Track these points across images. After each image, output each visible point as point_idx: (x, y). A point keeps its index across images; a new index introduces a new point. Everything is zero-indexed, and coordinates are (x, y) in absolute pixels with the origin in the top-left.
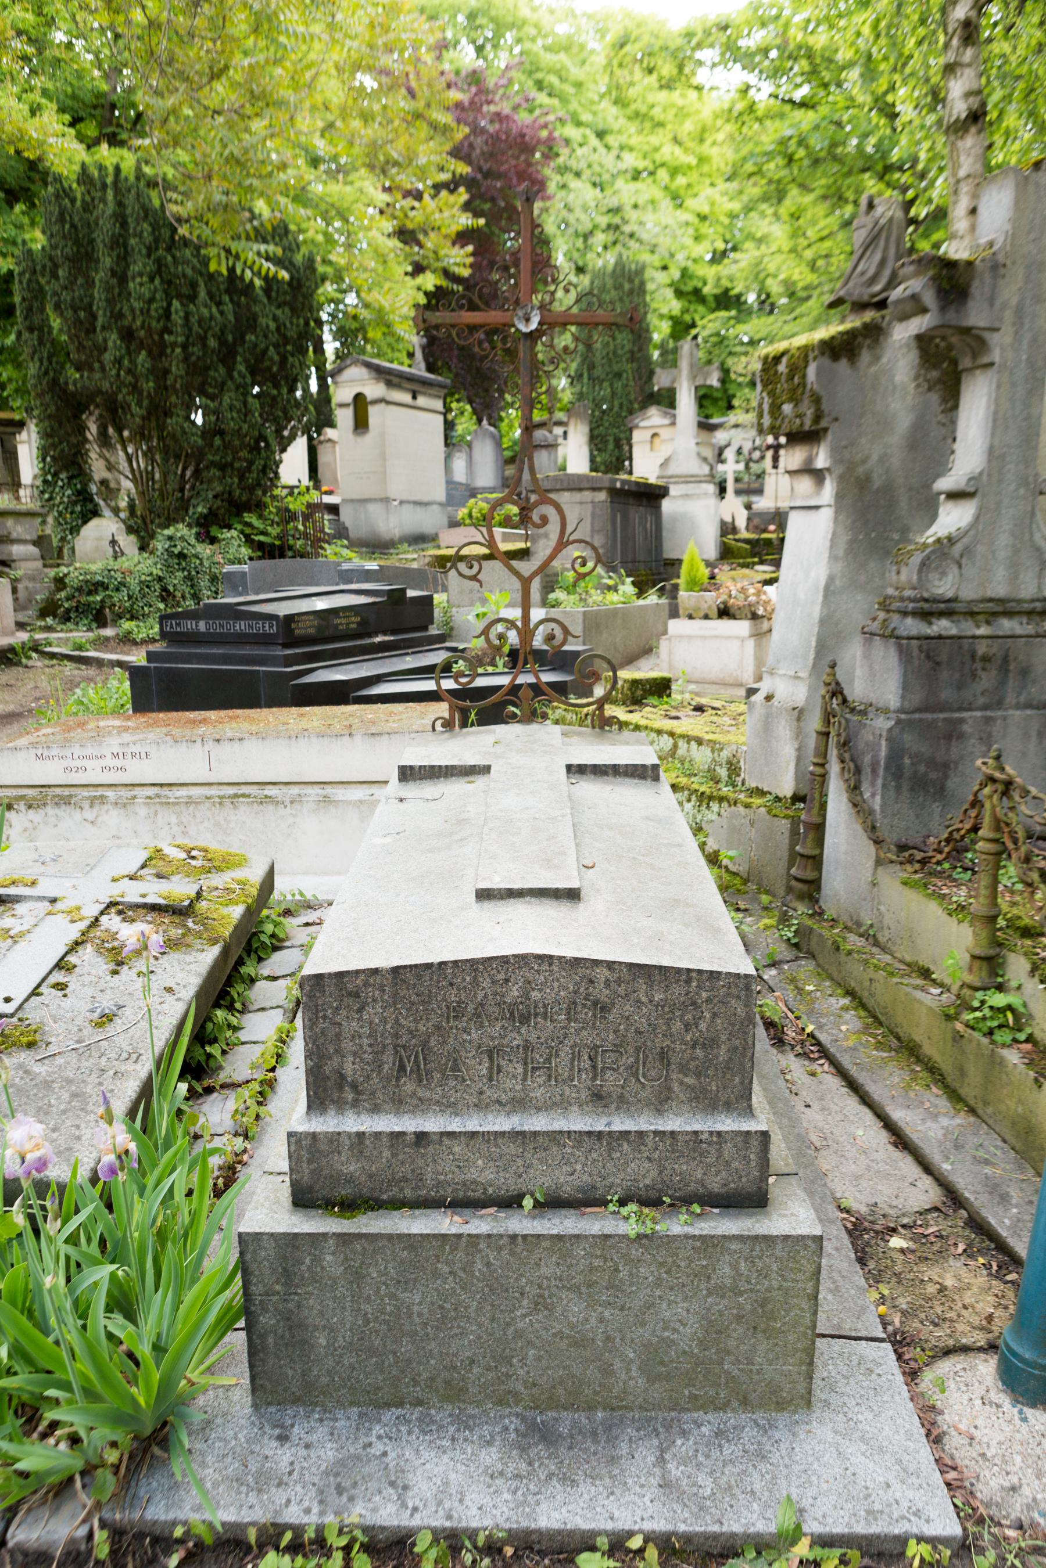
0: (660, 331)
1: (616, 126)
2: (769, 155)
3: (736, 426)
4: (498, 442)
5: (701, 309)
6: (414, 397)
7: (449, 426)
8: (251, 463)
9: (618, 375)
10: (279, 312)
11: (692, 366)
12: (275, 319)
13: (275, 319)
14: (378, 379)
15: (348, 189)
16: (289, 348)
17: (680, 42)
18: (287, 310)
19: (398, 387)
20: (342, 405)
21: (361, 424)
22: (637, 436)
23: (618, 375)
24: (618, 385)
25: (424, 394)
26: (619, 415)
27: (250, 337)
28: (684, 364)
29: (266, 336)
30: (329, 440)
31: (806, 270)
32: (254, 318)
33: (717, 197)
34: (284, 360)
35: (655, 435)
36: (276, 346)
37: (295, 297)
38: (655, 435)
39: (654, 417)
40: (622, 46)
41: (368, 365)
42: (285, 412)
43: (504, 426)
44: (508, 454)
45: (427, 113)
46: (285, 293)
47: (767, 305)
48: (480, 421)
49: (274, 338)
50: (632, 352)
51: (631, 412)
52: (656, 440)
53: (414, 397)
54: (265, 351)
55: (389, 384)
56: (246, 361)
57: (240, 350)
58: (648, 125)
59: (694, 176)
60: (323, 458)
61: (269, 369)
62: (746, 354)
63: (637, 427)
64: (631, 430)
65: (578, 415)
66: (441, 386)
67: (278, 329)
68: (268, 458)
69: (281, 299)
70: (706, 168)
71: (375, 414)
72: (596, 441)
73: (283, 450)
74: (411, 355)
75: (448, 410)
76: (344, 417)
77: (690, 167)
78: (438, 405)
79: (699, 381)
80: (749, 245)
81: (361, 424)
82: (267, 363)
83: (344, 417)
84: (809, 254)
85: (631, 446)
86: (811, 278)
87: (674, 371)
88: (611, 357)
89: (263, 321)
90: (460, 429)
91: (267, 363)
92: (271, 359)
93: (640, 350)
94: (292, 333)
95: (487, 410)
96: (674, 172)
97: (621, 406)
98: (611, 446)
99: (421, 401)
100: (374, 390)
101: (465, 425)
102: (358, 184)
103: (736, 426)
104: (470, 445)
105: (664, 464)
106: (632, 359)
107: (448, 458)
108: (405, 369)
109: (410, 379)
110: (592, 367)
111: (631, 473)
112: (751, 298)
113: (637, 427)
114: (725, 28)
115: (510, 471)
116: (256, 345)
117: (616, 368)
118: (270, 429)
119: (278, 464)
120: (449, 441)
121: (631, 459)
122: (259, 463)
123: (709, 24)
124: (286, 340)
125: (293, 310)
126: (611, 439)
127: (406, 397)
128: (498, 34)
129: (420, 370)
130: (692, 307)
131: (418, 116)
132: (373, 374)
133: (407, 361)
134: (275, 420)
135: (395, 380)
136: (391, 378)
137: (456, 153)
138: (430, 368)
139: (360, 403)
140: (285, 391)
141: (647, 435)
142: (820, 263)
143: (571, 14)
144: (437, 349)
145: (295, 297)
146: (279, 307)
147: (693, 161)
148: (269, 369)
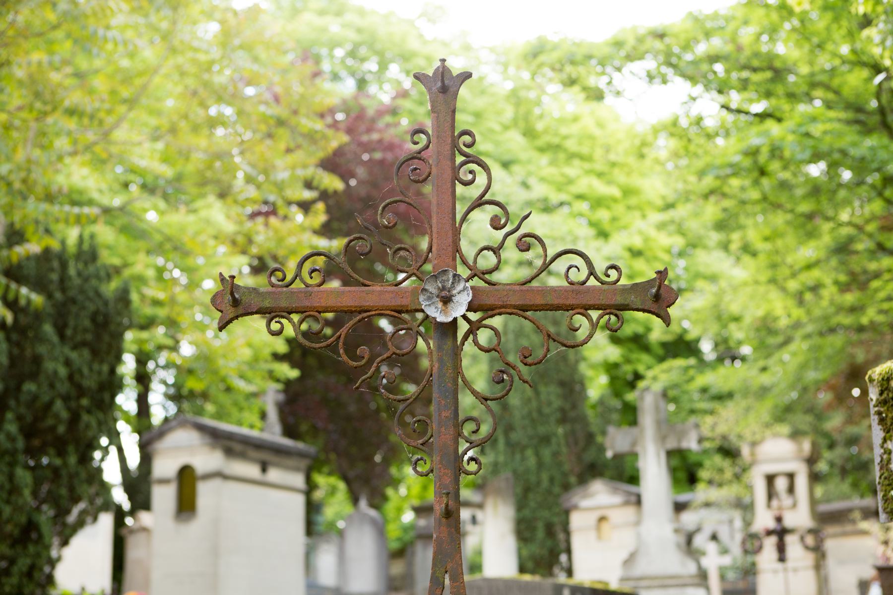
0: (597, 387)
1: (523, 156)
2: (736, 170)
3: (707, 505)
4: (381, 530)
5: (646, 358)
6: (264, 470)
7: (312, 509)
8: (12, 562)
9: (546, 440)
10: (74, 355)
11: (659, 423)
12: (68, 363)
13: (68, 363)
14: (213, 446)
15: (192, 218)
16: (85, 402)
17: (607, 50)
18: (86, 353)
19: (242, 456)
20: (164, 481)
21: (186, 506)
22: (576, 520)
23: (546, 440)
24: (546, 453)
25: (277, 465)
26: (549, 492)
27: (29, 387)
28: (647, 420)
29: (52, 386)
30: (145, 530)
31: (791, 303)
32: (37, 360)
33: (653, 233)
34: (75, 419)
35: (602, 519)
36: (66, 399)
37: (98, 337)
38: (602, 519)
39: (600, 496)
40: (535, 55)
41: (201, 428)
42: (72, 489)
43: (390, 508)
44: (394, 545)
45: (293, 120)
46: (86, 330)
47: (728, 354)
48: (355, 501)
49: (64, 387)
50: (562, 410)
51: (566, 487)
52: (605, 526)
53: (264, 470)
54: (49, 405)
55: (229, 452)
56: (19, 418)
57: (12, 403)
58: (562, 156)
59: (619, 209)
60: (134, 552)
61: (53, 429)
62: (711, 412)
63: (576, 507)
64: (567, 513)
65: (498, 492)
66: (301, 455)
67: (71, 377)
68: (38, 555)
69: (79, 338)
70: (633, 201)
71: (205, 493)
72: (524, 531)
73: (65, 543)
74: (263, 416)
75: (311, 486)
76: (164, 497)
77: (615, 200)
78: (298, 480)
79: (672, 444)
80: (700, 284)
81: (186, 506)
82: (50, 422)
83: (164, 497)
84: (793, 285)
85: (568, 533)
86: (798, 313)
87: (634, 431)
88: (536, 417)
89: (49, 366)
90: (329, 513)
91: (50, 422)
92: (57, 416)
93: (574, 407)
94: (90, 382)
95: (368, 486)
96: (598, 203)
97: (552, 480)
98: (540, 534)
99: (274, 475)
100: (206, 459)
101: (337, 505)
102: (203, 213)
103: (707, 505)
104: (341, 534)
105: (630, 561)
106: (564, 419)
107: (309, 555)
108: (255, 433)
109: (259, 445)
110: (509, 429)
111: (570, 572)
112: (706, 347)
113: (576, 507)
114: (661, 36)
115: (397, 568)
116: (35, 398)
117: (542, 430)
118: (48, 511)
119: (53, 563)
120: (310, 528)
121: (569, 551)
122: (23, 563)
123: (642, 31)
124: (81, 391)
125: (95, 353)
126: (540, 525)
127: (252, 470)
128: (383, 66)
129: (274, 434)
130: (634, 356)
131: (281, 122)
132: (208, 440)
133: (258, 423)
134: (53, 499)
135: (238, 447)
136: (231, 445)
137: (331, 164)
138: (289, 431)
139: (186, 478)
140: (73, 460)
141: (593, 517)
142: (808, 296)
143: (467, 48)
144: (295, 408)
145: (98, 337)
146: (75, 347)
147: (615, 192)
148: (53, 429)
